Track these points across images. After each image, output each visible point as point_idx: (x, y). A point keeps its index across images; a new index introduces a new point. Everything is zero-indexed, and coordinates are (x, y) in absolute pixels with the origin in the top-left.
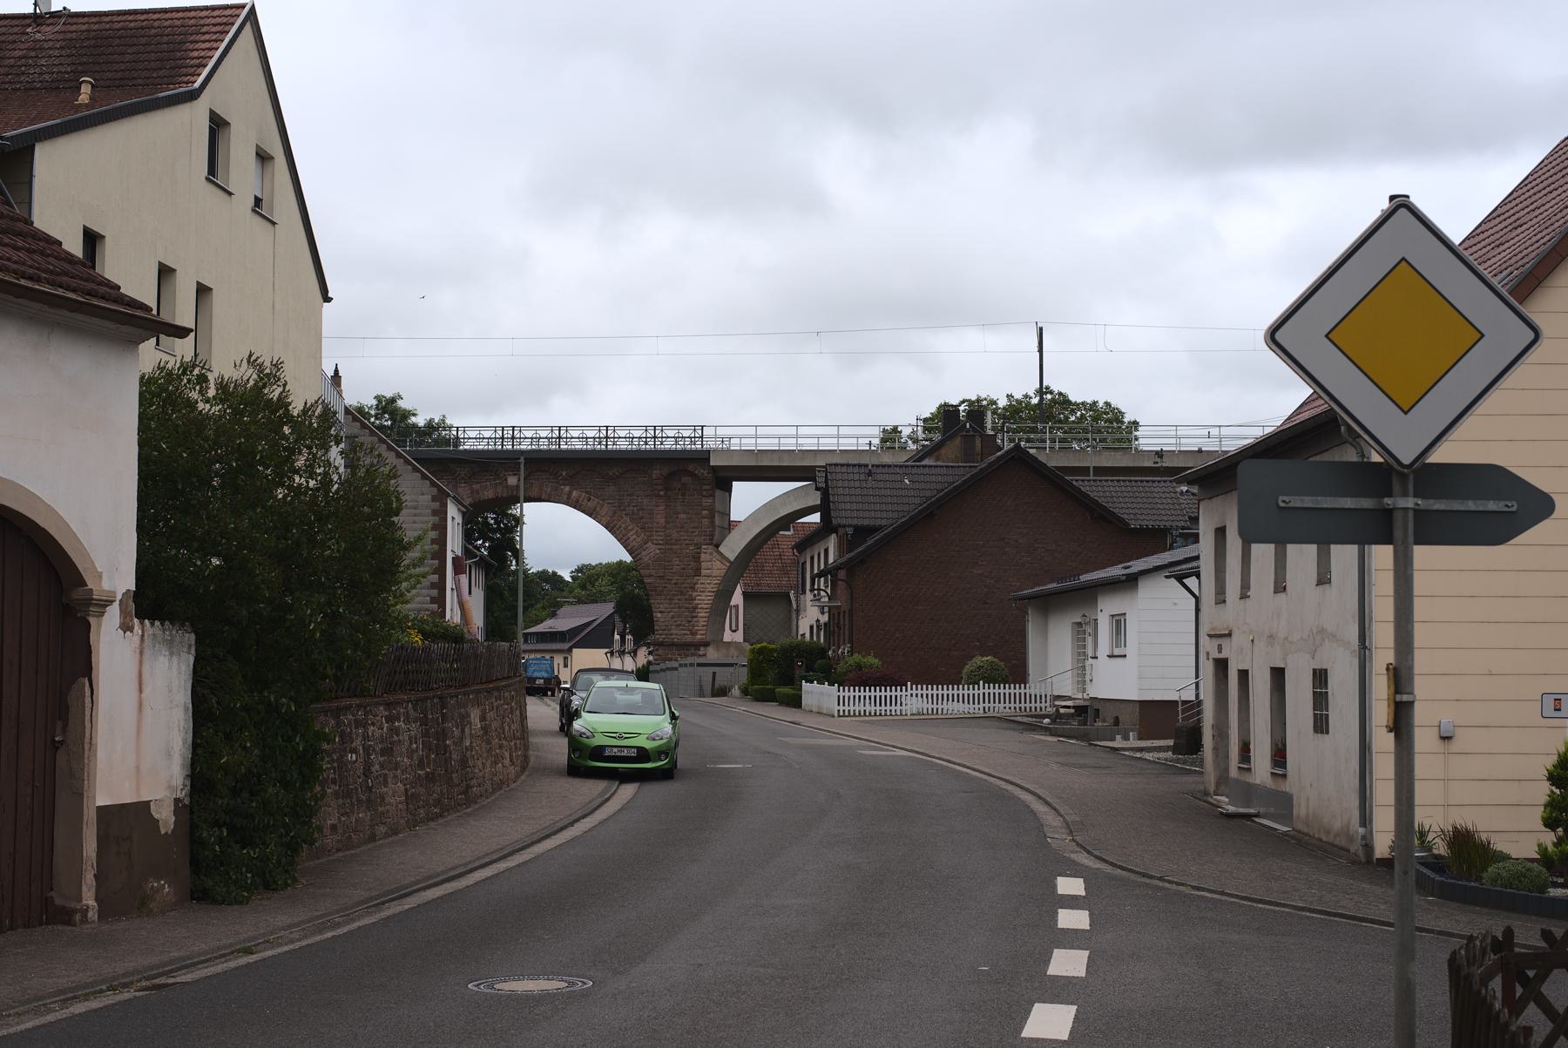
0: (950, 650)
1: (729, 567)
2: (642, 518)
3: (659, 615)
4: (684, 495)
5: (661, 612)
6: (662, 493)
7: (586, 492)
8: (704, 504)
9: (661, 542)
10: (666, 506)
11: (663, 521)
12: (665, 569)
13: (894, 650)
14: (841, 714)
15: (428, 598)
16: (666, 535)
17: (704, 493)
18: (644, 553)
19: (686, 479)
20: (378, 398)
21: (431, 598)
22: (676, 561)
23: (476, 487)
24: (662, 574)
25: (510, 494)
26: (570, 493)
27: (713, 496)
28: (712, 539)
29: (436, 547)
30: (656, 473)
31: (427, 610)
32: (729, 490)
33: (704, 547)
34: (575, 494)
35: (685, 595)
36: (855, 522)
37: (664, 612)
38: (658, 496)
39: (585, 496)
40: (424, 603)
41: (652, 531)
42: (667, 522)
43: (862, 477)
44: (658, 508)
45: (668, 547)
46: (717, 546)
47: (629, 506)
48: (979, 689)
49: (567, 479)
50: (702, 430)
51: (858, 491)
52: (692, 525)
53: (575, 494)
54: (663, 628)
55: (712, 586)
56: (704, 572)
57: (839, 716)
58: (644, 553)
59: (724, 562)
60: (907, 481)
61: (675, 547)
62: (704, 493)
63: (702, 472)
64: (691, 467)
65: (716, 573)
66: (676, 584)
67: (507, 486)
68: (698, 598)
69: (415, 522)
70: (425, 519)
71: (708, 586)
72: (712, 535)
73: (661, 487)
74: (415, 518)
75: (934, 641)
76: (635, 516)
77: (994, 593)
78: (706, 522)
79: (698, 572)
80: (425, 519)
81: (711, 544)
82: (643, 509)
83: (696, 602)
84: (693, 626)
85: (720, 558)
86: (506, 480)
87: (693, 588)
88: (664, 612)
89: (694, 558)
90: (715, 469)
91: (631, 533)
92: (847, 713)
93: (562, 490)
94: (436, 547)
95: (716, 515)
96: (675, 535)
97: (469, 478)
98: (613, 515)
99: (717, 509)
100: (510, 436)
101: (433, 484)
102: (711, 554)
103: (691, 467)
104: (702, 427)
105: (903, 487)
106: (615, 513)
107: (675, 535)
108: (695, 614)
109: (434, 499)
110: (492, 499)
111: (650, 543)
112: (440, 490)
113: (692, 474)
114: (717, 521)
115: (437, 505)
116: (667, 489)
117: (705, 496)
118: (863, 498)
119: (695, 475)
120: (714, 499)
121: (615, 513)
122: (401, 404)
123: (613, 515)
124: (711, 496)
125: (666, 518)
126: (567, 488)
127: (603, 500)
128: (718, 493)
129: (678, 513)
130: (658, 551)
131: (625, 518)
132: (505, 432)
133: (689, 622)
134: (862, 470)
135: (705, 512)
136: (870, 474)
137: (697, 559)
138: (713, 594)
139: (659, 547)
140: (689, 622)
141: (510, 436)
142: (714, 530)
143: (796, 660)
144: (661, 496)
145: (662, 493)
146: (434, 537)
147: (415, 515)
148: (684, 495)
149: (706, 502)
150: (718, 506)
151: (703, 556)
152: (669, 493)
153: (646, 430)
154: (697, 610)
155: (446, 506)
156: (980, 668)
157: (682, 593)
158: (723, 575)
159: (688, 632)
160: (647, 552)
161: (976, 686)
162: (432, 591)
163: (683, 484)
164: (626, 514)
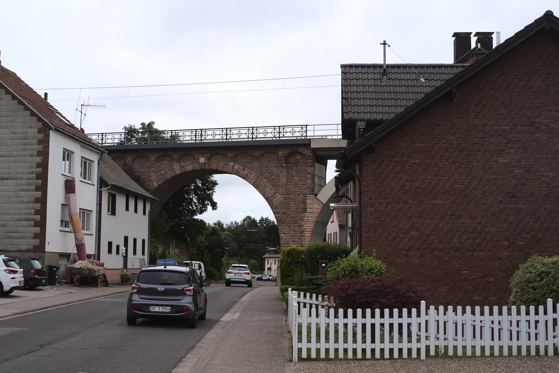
0: (474, 250)
1: (323, 207)
2: (274, 179)
3: (283, 235)
4: (297, 166)
5: (284, 234)
6: (284, 165)
7: (243, 166)
8: (308, 171)
9: (284, 193)
10: (287, 172)
11: (285, 181)
12: (286, 209)
13: (408, 250)
14: (304, 355)
15: (33, 210)
16: (287, 190)
17: (308, 164)
18: (274, 200)
19: (298, 157)
20: (143, 124)
21: (35, 210)
22: (292, 204)
23: (183, 164)
24: (285, 212)
25: (200, 167)
26: (233, 167)
27: (313, 166)
28: (313, 191)
29: (39, 170)
30: (281, 153)
31: (32, 220)
32: (325, 165)
33: (308, 196)
34: (236, 167)
35: (297, 223)
36: (367, 117)
37: (286, 234)
38: (282, 167)
39: (242, 168)
40: (30, 215)
41: (279, 187)
42: (288, 182)
43: (377, 76)
44: (282, 174)
45: (288, 196)
46: (316, 195)
47: (266, 173)
48: (545, 313)
49: (231, 159)
50: (306, 127)
51: (373, 89)
52: (302, 183)
53: (236, 167)
54: (285, 243)
55: (313, 218)
56: (308, 210)
57: (300, 359)
58: (274, 200)
59: (320, 204)
60: (422, 80)
61: (292, 196)
62: (308, 164)
63: (307, 152)
64: (300, 150)
65: (315, 210)
66: (293, 217)
67: (199, 163)
68: (305, 225)
69: (24, 150)
70: (32, 147)
71: (310, 218)
72: (313, 189)
73: (284, 162)
74: (26, 147)
75: (455, 240)
76: (270, 179)
77: (523, 184)
78: (309, 181)
79: (305, 210)
80: (32, 147)
81: (312, 194)
82: (274, 175)
83: (304, 227)
84: (302, 242)
85: (317, 202)
86: (199, 160)
87: (302, 220)
88: (286, 234)
89: (303, 202)
90: (314, 150)
91: (267, 188)
92: (313, 355)
93: (229, 165)
94: (39, 170)
95: (316, 177)
96: (292, 189)
97: (179, 159)
98: (257, 178)
99: (316, 174)
100: (199, 134)
101: (39, 119)
102: (312, 199)
103: (300, 150)
104: (307, 125)
105: (418, 85)
106: (258, 177)
107: (292, 189)
108: (303, 235)
109: (40, 131)
110: (192, 170)
111: (278, 194)
112: (44, 123)
113: (301, 154)
114: (317, 181)
115: (41, 136)
116: (287, 163)
117: (308, 166)
118: (377, 94)
119: (303, 154)
120: (314, 168)
121: (258, 177)
122: (155, 126)
123: (257, 178)
124: (312, 166)
125: (287, 179)
126: (232, 164)
127: (252, 170)
128: (317, 165)
129: (293, 176)
130: (282, 199)
131: (264, 180)
132: (197, 132)
133: (300, 239)
134: (378, 70)
135: (308, 176)
136: (385, 73)
137: (304, 202)
138: (313, 223)
139: (283, 196)
140: (300, 239)
141: (199, 134)
142: (314, 186)
143: (320, 261)
144: (284, 167)
145: (284, 165)
146: (38, 162)
147: (25, 144)
148: (297, 166)
149: (310, 170)
150: (317, 172)
151: (308, 201)
152: (289, 165)
153: (275, 129)
154: (304, 232)
155: (48, 136)
156: (541, 275)
157: (296, 223)
158: (319, 212)
159: (300, 245)
160: (276, 199)
161: (541, 308)
162: (36, 204)
163: (297, 160)
164: (264, 178)
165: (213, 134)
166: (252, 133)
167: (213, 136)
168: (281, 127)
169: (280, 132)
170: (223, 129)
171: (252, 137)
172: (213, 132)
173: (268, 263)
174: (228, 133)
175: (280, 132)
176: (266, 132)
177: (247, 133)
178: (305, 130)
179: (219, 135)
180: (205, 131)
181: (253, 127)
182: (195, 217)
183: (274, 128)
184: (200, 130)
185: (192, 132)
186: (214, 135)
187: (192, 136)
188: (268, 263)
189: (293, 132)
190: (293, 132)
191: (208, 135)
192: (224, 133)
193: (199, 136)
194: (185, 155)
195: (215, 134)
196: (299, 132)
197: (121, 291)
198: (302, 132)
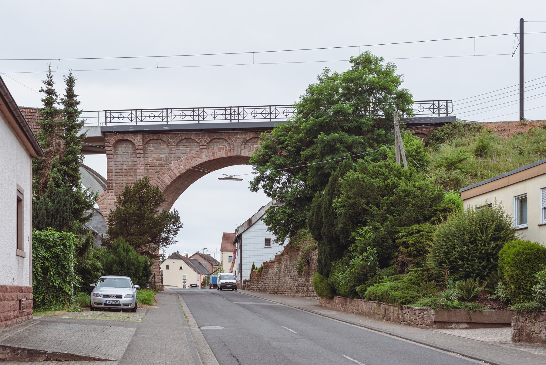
132: (232, 111)
165: (213, 114)
166: (166, 116)
167: (120, 119)
168: (200, 109)
169: (271, 113)
170: (194, 109)
171: (166, 120)
172: (420, 105)
173: (235, 271)
174: (200, 114)
175: (200, 115)
176: (255, 112)
177: (245, 115)
178: (137, 118)
179: (190, 115)
180: (110, 113)
181: (167, 109)
182: (363, 221)
183: (161, 110)
184: (237, 108)
185: (131, 112)
186: (215, 115)
187: (203, 115)
188: (235, 271)
189: (286, 113)
190: (286, 113)
191: (207, 115)
192: (195, 114)
193: (236, 115)
194: (211, 140)
195: (122, 116)
196: (261, 114)
197: (385, 334)
198: (265, 113)
